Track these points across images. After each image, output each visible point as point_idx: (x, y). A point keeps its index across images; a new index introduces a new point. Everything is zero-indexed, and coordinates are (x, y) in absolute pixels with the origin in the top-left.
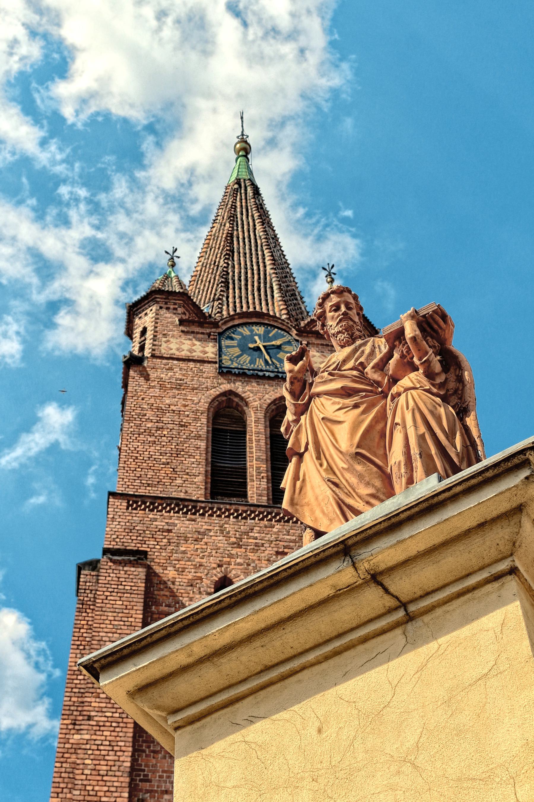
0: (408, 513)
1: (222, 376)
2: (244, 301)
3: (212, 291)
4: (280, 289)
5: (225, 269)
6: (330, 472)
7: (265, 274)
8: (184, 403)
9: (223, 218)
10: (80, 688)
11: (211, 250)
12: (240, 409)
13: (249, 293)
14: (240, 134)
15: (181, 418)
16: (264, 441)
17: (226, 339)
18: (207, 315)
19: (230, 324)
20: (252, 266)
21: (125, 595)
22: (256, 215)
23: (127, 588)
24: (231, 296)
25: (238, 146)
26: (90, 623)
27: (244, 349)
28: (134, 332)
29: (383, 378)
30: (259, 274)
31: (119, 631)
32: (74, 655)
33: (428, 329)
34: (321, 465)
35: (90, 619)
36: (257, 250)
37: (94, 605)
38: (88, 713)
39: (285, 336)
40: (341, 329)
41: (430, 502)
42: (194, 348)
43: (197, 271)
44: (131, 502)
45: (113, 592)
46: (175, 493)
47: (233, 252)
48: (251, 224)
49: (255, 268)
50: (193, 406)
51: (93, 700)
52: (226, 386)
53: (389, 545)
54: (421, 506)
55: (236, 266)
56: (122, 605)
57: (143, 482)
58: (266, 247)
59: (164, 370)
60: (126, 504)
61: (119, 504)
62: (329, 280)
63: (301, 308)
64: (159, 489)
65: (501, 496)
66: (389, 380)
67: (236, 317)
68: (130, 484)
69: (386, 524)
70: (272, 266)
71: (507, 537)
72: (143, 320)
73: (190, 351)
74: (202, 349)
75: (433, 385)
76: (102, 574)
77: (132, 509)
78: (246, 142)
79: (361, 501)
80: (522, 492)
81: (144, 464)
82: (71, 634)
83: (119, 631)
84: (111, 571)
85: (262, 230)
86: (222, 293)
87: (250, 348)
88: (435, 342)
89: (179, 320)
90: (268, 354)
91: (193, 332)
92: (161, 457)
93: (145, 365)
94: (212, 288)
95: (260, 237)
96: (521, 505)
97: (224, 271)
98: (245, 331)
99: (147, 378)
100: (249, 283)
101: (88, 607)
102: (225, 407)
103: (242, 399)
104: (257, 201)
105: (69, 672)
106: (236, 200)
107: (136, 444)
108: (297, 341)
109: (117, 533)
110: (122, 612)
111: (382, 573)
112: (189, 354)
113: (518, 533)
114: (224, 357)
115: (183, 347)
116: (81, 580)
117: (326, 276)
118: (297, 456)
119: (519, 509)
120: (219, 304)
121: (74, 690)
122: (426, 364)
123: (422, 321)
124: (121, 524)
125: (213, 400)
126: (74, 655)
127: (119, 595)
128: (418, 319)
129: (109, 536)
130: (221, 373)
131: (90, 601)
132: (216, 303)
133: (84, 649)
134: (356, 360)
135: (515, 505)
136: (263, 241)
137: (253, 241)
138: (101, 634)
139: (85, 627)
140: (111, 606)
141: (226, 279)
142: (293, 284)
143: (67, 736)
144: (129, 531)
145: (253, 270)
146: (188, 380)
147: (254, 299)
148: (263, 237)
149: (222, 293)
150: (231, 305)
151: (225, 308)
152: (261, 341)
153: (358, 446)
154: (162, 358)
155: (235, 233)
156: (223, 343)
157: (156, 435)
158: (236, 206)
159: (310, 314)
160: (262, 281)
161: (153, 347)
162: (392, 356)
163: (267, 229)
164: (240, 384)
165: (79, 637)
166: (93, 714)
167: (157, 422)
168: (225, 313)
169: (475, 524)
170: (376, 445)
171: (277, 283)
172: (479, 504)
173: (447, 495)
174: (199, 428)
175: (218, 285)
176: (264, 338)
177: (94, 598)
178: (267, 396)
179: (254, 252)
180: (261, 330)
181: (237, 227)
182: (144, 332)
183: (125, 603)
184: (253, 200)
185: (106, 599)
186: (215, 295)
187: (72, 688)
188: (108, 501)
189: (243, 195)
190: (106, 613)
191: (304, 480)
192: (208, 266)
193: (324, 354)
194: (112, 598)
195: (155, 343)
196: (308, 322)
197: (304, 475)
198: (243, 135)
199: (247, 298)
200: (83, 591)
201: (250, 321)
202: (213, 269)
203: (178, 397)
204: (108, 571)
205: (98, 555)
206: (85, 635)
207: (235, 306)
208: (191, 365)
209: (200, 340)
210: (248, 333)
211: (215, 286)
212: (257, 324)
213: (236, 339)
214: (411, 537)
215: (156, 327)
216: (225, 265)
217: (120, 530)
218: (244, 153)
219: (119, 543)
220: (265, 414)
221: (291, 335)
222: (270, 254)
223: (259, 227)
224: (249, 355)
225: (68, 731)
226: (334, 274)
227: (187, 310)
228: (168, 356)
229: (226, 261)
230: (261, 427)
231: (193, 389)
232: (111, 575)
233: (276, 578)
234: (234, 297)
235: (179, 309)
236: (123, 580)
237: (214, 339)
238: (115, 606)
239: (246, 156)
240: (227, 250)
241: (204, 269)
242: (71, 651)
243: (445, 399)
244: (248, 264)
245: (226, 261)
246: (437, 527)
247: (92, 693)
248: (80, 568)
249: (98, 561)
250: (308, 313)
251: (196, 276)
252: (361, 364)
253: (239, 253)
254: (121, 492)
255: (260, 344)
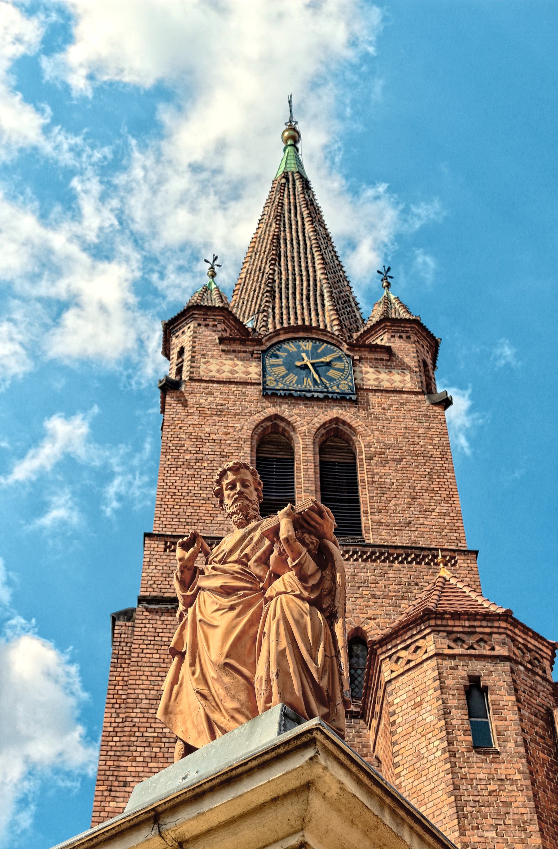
0: (210, 784)
1: (266, 399)
2: (292, 312)
3: (256, 301)
4: (331, 297)
5: (270, 277)
6: (202, 681)
7: (315, 280)
8: (225, 430)
9: (269, 217)
10: (115, 751)
11: (256, 254)
12: (287, 435)
13: (298, 302)
14: (288, 120)
15: (222, 447)
16: (313, 470)
17: (271, 357)
18: (250, 330)
19: (275, 340)
20: (301, 271)
21: (163, 647)
22: (305, 213)
23: (164, 639)
24: (277, 306)
25: (286, 134)
26: (126, 679)
27: (290, 367)
28: (172, 352)
29: (265, 573)
30: (308, 280)
31: (156, 688)
32: (109, 715)
33: (305, 525)
34: (193, 673)
35: (126, 674)
36: (306, 253)
37: (130, 659)
38: (124, 779)
39: (335, 351)
40: (235, 509)
41: (229, 774)
42: (236, 368)
43: (241, 279)
44: (168, 544)
45: (150, 644)
46: (216, 532)
47: (280, 256)
48: (300, 223)
49: (304, 273)
50: (235, 433)
51: (129, 764)
52: (271, 410)
53: (191, 816)
54: (221, 778)
55: (283, 272)
56: (160, 658)
57: (181, 520)
58: (316, 249)
59: (203, 395)
60: (163, 546)
61: (156, 546)
62: (385, 284)
63: (355, 316)
64: (199, 528)
65: (289, 776)
66: (270, 575)
67: (282, 332)
68: (167, 523)
69: (191, 794)
70: (322, 271)
71: (296, 813)
72: (180, 339)
73: (232, 372)
74: (244, 369)
75: (305, 588)
76: (137, 625)
77: (170, 551)
78: (294, 129)
79: (226, 715)
80: (308, 771)
81: (182, 501)
82: (106, 691)
83: (156, 688)
84: (147, 621)
85: (312, 229)
86: (267, 304)
87: (298, 367)
88: (313, 538)
89: (219, 338)
90: (317, 372)
91: (234, 351)
92: (201, 492)
93: (183, 390)
94: (257, 298)
95: (310, 238)
96: (309, 782)
97: (269, 278)
98: (291, 347)
99: (185, 404)
100: (298, 291)
101: (123, 661)
102: (271, 433)
103: (289, 423)
104: (307, 197)
105: (104, 734)
106: (283, 196)
107: (173, 479)
108: (348, 356)
109: (154, 579)
110: (160, 667)
111: (187, 841)
112: (230, 375)
113: (306, 810)
114: (268, 378)
115: (223, 368)
116: (116, 631)
117: (382, 280)
118: (179, 656)
119: (308, 786)
120: (265, 316)
121: (110, 753)
122: (298, 568)
123: (298, 519)
124: (158, 568)
125: (257, 426)
126: (109, 715)
127: (156, 647)
128: (294, 516)
129: (145, 582)
130: (265, 396)
131: (125, 654)
132: (261, 316)
133: (120, 708)
134: (241, 552)
135: (303, 782)
136: (313, 242)
137: (301, 243)
138: (137, 691)
139: (121, 683)
140: (148, 660)
141: (272, 287)
142: (347, 288)
143: (103, 804)
144: (167, 576)
145: (301, 276)
146: (229, 405)
147: (303, 309)
148: (312, 238)
149: (267, 304)
150: (277, 317)
151: (270, 320)
152: (309, 358)
153: (227, 656)
154: (201, 381)
155: (282, 234)
156: (267, 362)
157: (195, 467)
158: (283, 204)
159: (365, 322)
160: (312, 288)
161: (191, 370)
162: (272, 552)
163: (317, 228)
164: (287, 406)
165: (114, 694)
166: (129, 779)
167: (196, 453)
168: (270, 326)
169: (268, 798)
170: (246, 652)
171: (328, 289)
172: (269, 782)
173: (244, 768)
174: (242, 458)
175: (263, 295)
176: (312, 354)
177: (130, 651)
178: (316, 419)
179: (302, 255)
180: (308, 346)
181: (285, 228)
182: (181, 352)
183: (162, 656)
184: (302, 196)
185: (142, 652)
186: (260, 305)
187: (107, 751)
188: (144, 544)
189: (291, 190)
190: (142, 668)
191: (181, 685)
192: (253, 273)
193: (379, 369)
194: (148, 651)
195: (193, 364)
196: (361, 334)
197: (183, 679)
198: (290, 121)
199: (295, 308)
200: (118, 644)
201: (296, 336)
202: (258, 276)
203: (219, 424)
204: (144, 622)
205: (133, 603)
206: (120, 692)
207: (282, 318)
208: (233, 387)
209: (242, 360)
210: (295, 350)
211: (260, 295)
212: (304, 339)
213: (282, 357)
214: (210, 810)
215: (194, 347)
216: (271, 272)
217: (157, 575)
218: (293, 143)
219: (156, 590)
220: (314, 440)
221: (342, 351)
222: (320, 257)
223: (308, 226)
224: (296, 375)
225: (103, 798)
226: (391, 277)
227: (228, 326)
228: (208, 379)
229: (272, 267)
230: (310, 455)
231: (235, 415)
232: (148, 626)
233: (95, 841)
234: (281, 308)
235: (218, 325)
236: (161, 631)
237: (258, 358)
238: (151, 660)
239: (294, 146)
240: (273, 254)
241: (248, 276)
242: (106, 710)
243: (315, 603)
244: (297, 269)
245: (272, 267)
246: (232, 802)
247: (129, 757)
248: (114, 620)
249: (133, 610)
250: (363, 320)
251: (240, 284)
252: (246, 555)
253: (287, 257)
254: (157, 533)
255: (308, 362)
